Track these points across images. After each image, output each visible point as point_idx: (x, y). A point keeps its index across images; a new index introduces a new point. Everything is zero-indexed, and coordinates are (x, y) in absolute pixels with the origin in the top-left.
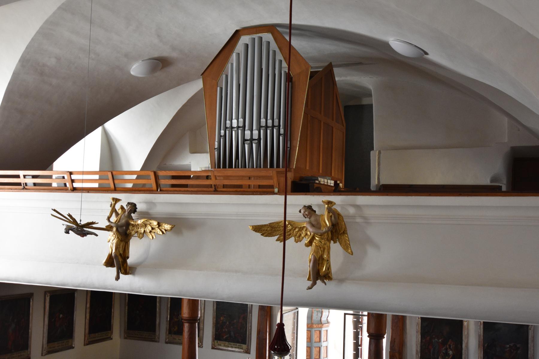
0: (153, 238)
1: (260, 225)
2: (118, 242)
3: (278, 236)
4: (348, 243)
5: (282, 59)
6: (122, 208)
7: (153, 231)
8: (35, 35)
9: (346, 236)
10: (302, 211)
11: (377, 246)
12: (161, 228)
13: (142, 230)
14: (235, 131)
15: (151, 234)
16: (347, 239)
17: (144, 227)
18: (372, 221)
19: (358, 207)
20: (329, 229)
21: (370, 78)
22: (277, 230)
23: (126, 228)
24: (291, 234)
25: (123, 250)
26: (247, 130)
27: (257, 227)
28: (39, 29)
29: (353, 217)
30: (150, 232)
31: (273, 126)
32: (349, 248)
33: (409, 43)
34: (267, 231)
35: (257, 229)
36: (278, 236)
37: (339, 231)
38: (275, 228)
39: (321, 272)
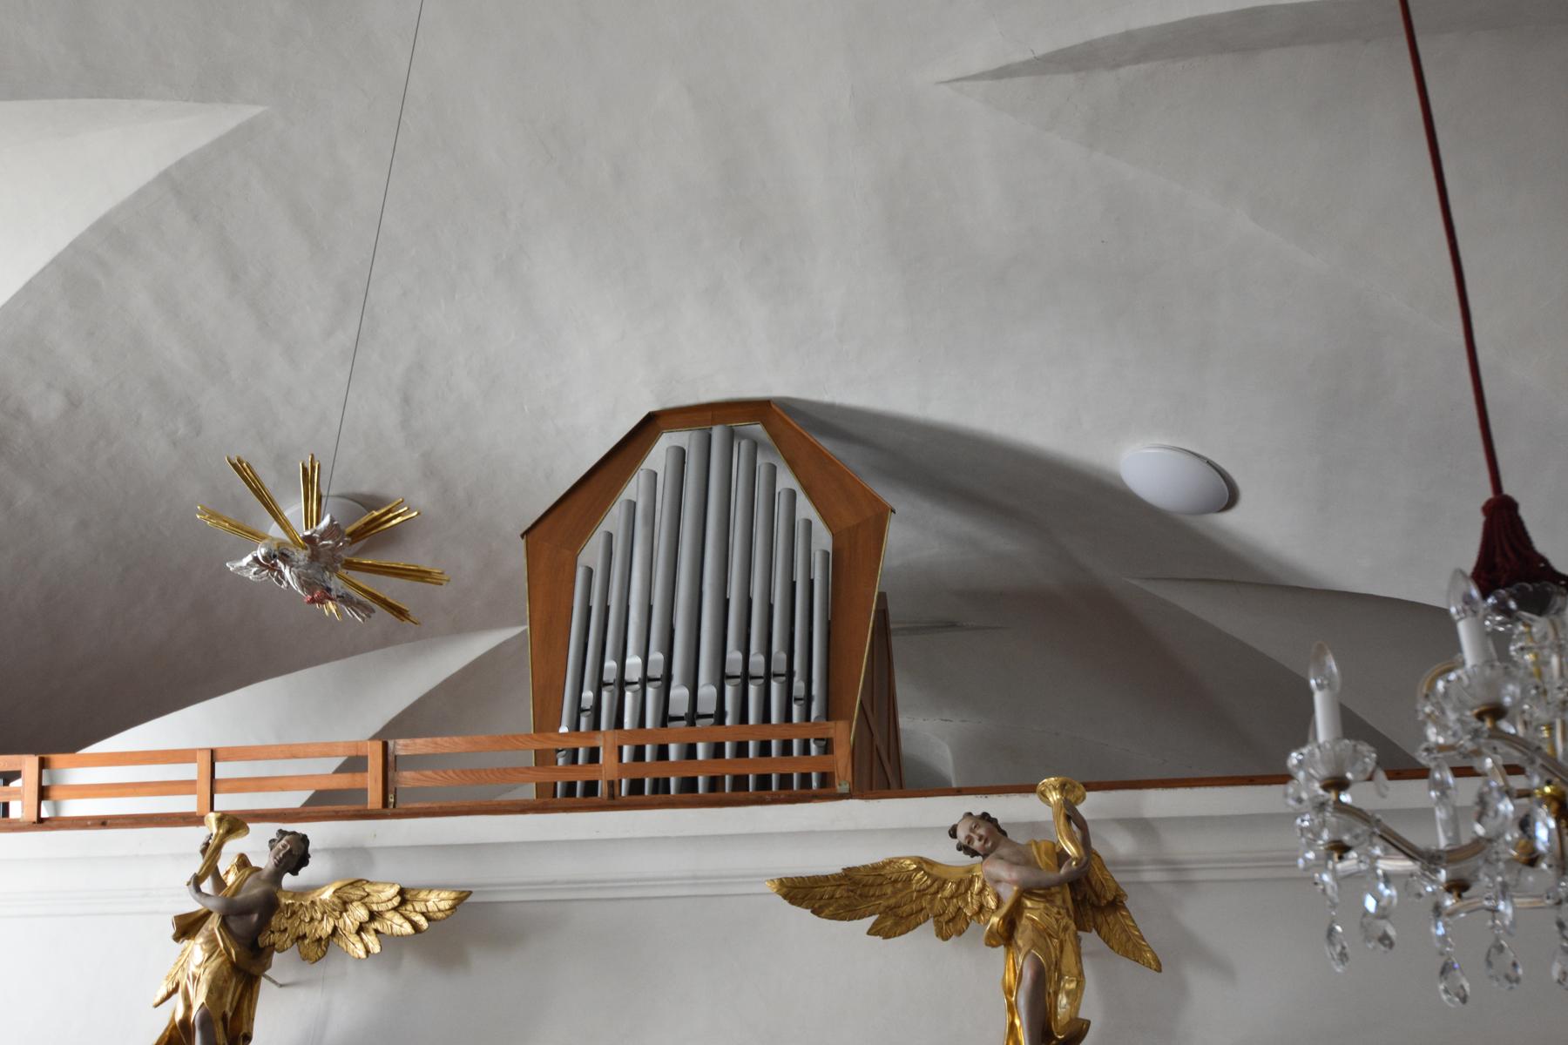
0: (368, 952)
1: (808, 878)
2: (224, 968)
3: (873, 919)
4: (1134, 935)
5: (795, 485)
6: (243, 862)
7: (376, 925)
8: (43, 270)
9: (1122, 915)
10: (962, 834)
11: (1220, 967)
12: (409, 907)
13: (326, 927)
14: (634, 692)
15: (362, 939)
16: (1131, 924)
17: (337, 914)
18: (1199, 876)
19: (1142, 827)
20: (1080, 866)
21: (942, 720)
22: (873, 896)
23: (259, 918)
24: (922, 909)
25: (235, 1004)
26: (677, 687)
27: (799, 883)
28: (66, 250)
29: (1132, 864)
30: (361, 929)
31: (768, 676)
32: (1147, 949)
33: (1189, 452)
34: (833, 900)
35: (796, 890)
36: (873, 919)
37: (1094, 898)
38: (864, 886)
39: (1056, 1029)
